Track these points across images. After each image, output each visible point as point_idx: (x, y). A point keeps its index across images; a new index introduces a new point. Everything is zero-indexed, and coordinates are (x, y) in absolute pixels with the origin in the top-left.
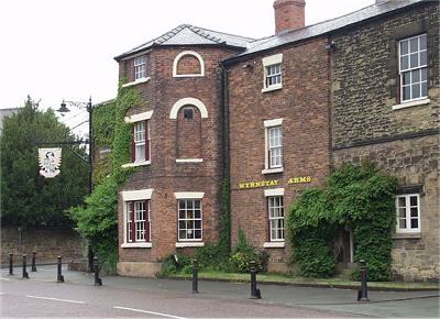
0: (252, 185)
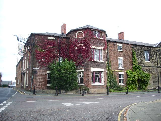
0: (115, 71)
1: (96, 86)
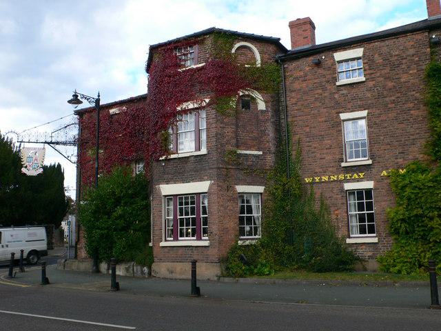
0: (325, 178)
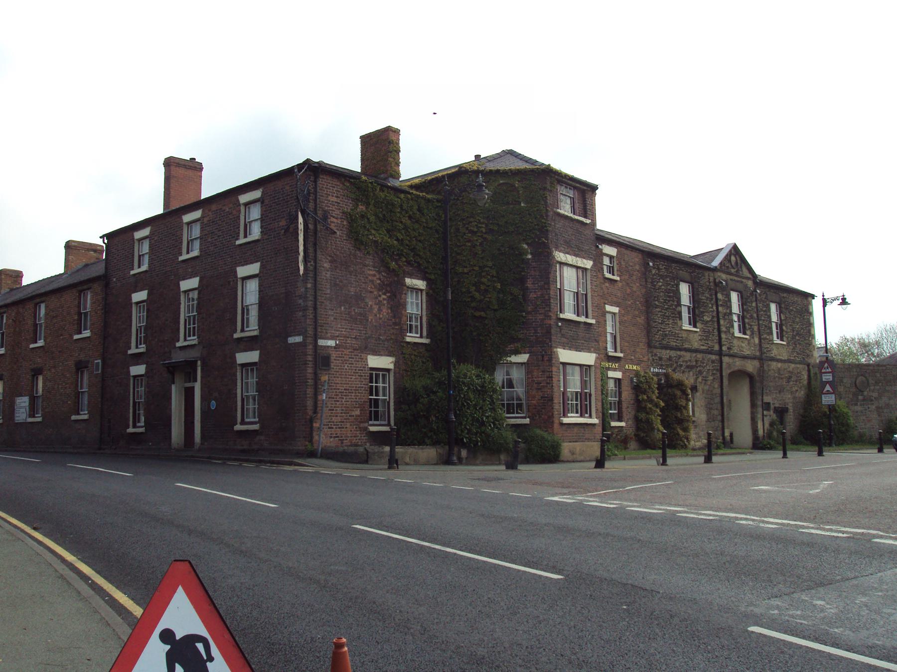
1: (576, 429)
